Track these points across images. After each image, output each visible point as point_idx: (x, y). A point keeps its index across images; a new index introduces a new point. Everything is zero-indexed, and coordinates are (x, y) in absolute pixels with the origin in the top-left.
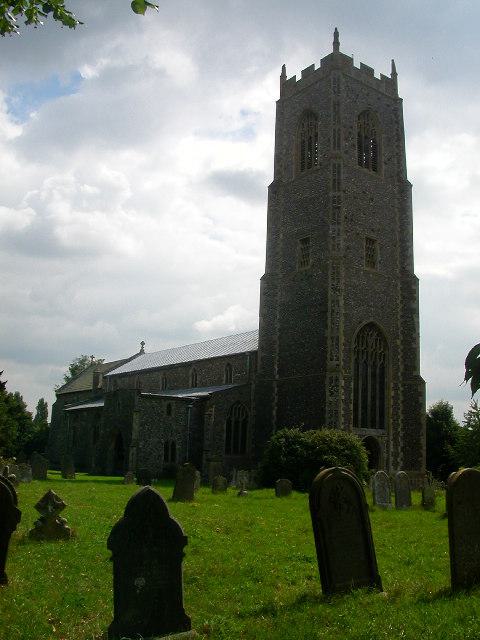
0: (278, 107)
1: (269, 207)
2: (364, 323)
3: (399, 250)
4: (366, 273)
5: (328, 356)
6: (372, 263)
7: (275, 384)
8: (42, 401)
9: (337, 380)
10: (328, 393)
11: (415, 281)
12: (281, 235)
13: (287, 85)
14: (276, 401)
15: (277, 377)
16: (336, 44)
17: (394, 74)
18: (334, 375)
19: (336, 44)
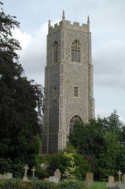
0: (47, 37)
1: (45, 75)
2: (73, 116)
3: (88, 89)
4: (74, 99)
5: (59, 128)
6: (76, 95)
7: (48, 136)
8: (17, 24)
9: (61, 135)
10: (59, 140)
11: (93, 99)
12: (49, 85)
13: (50, 29)
14: (48, 141)
15: (48, 133)
16: (63, 17)
17: (88, 22)
18: (61, 134)
19: (63, 17)
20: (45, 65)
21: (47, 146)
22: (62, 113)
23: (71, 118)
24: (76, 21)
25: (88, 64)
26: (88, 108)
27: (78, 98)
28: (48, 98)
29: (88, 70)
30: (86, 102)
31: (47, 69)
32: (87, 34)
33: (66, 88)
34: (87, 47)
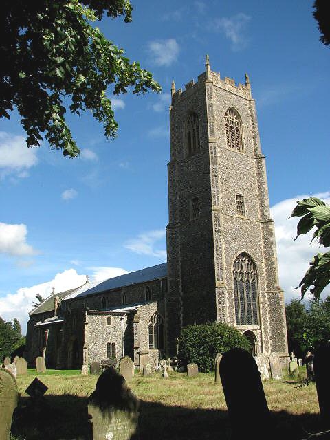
6: (242, 213)
7: (180, 298)
9: (223, 293)
10: (217, 303)
14: (182, 310)
15: (181, 294)
18: (221, 290)
20: (169, 159)
21: (179, 319)
22: (219, 244)
23: (235, 258)
24: (63, 155)
25: (256, 156)
26: (263, 240)
27: (243, 217)
28: (178, 221)
29: (256, 165)
30: (259, 226)
31: (171, 165)
32: (248, 102)
33: (221, 195)
34: (250, 124)
